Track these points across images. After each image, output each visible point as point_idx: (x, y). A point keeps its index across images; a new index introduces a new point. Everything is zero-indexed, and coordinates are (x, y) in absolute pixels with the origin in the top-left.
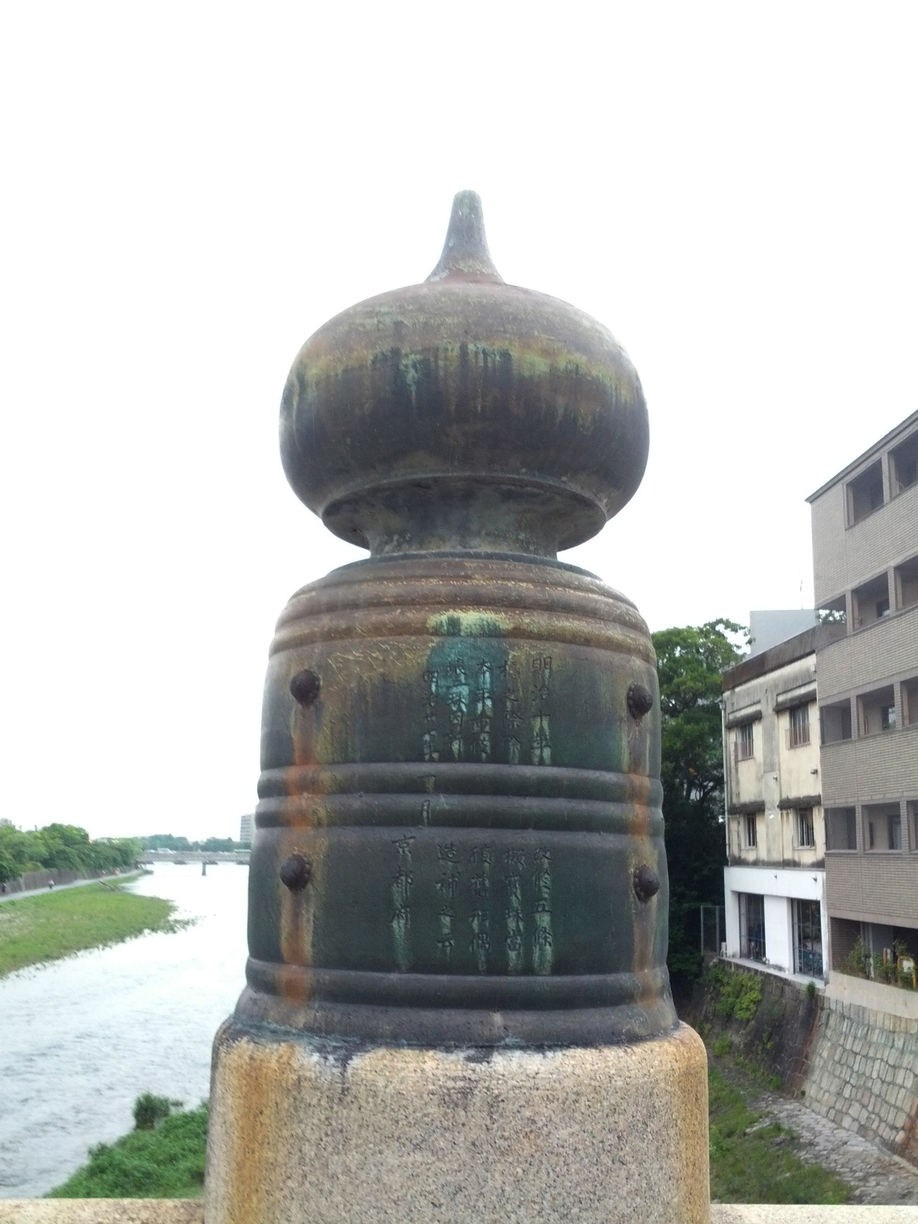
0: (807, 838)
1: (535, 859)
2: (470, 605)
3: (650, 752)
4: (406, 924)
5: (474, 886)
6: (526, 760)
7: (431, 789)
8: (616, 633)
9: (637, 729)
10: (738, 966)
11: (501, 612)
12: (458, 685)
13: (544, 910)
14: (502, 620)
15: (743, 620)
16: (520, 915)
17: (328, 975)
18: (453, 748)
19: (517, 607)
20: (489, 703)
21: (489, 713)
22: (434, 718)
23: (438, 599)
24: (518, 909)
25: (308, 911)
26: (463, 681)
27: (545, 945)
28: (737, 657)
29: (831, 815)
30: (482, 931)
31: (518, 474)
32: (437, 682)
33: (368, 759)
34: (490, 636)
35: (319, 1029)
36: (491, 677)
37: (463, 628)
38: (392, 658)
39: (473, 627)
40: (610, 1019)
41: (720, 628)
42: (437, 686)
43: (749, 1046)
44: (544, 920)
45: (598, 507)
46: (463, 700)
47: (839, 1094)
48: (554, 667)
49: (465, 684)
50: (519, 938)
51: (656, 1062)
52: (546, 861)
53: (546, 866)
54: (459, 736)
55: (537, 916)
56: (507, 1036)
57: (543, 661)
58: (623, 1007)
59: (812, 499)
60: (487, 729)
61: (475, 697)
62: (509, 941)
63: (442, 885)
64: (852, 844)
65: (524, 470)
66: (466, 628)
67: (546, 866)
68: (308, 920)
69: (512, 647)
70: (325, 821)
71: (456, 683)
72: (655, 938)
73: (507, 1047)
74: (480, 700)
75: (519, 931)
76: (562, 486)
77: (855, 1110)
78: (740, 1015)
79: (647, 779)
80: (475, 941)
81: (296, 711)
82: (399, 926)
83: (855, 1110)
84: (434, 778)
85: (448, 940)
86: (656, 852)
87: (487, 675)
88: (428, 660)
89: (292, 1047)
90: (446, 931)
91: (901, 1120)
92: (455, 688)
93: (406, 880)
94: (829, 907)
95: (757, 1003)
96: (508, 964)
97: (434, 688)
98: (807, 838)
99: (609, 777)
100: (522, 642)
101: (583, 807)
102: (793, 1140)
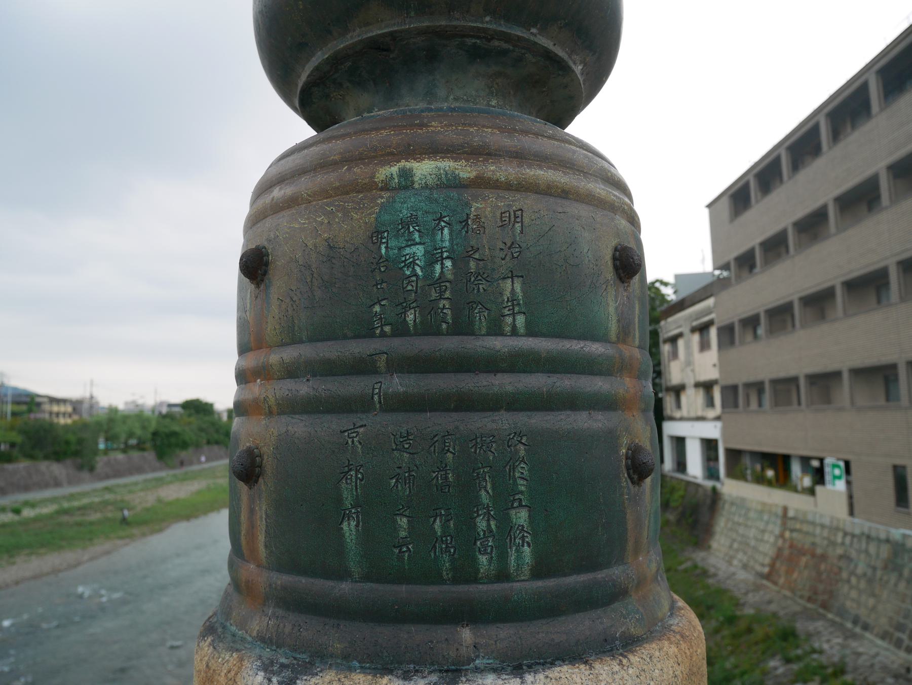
0: (710, 403)
1: (509, 447)
2: (425, 154)
3: (639, 321)
4: (357, 526)
5: (435, 481)
6: (496, 330)
7: (383, 369)
8: (599, 189)
9: (625, 294)
10: (672, 478)
11: (461, 159)
12: (411, 245)
13: (521, 505)
14: (465, 170)
15: (670, 279)
16: (492, 513)
17: (282, 579)
18: (408, 319)
19: (480, 154)
20: (448, 263)
21: (450, 276)
22: (384, 285)
23: (388, 150)
24: (488, 506)
25: (261, 509)
26: (418, 240)
27: (523, 546)
28: (668, 302)
29: (724, 389)
30: (444, 534)
31: (482, 22)
32: (387, 243)
33: (313, 339)
34: (448, 187)
35: (271, 639)
36: (451, 234)
37: (416, 179)
38: (337, 220)
39: (429, 177)
40: (601, 623)
41: (657, 285)
42: (387, 248)
43: (679, 522)
44: (521, 517)
45: (573, 71)
46: (417, 262)
47: (731, 547)
48: (526, 220)
49: (420, 244)
50: (491, 540)
51: (657, 671)
52: (522, 447)
53: (522, 453)
54: (414, 305)
55: (513, 512)
56: (477, 657)
57: (512, 213)
58: (616, 605)
59: (709, 206)
60: (447, 294)
61: (433, 258)
62: (478, 543)
63: (397, 481)
64: (736, 405)
65: (488, 19)
66: (421, 179)
67: (522, 453)
68: (261, 517)
69: (475, 198)
70: (275, 408)
71: (409, 243)
72: (649, 522)
73: (477, 670)
74: (438, 261)
75: (491, 531)
76: (532, 38)
77: (740, 556)
78: (673, 504)
79: (637, 349)
80: (437, 545)
81: (250, 293)
82: (349, 528)
83: (740, 556)
84: (386, 356)
85: (406, 545)
86: (648, 428)
87: (446, 231)
88: (376, 219)
89: (241, 660)
90: (403, 534)
91: (767, 561)
92: (409, 249)
93: (356, 476)
94: (725, 442)
95: (683, 497)
96: (478, 570)
97: (383, 251)
98: (710, 403)
99: (595, 348)
100: (487, 192)
101: (565, 383)
102: (705, 573)
